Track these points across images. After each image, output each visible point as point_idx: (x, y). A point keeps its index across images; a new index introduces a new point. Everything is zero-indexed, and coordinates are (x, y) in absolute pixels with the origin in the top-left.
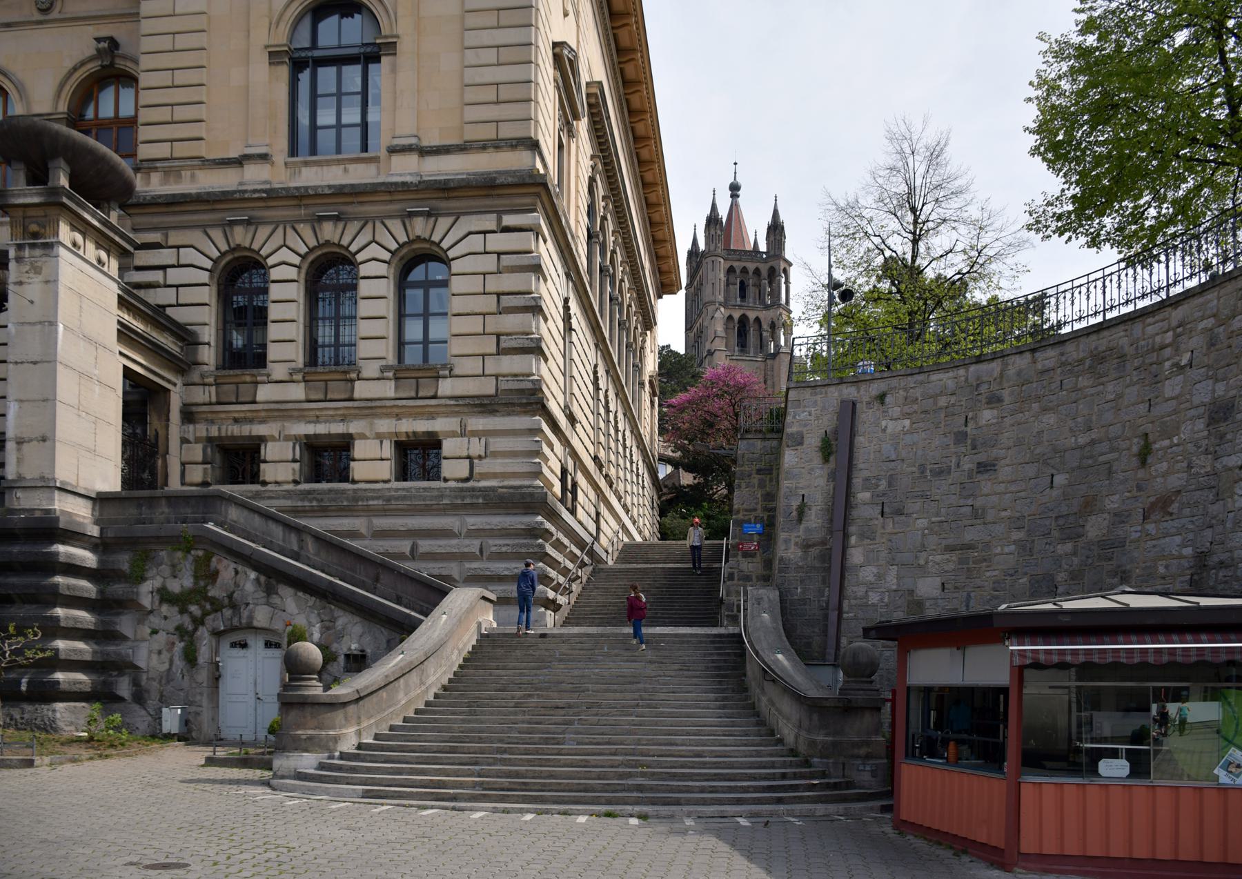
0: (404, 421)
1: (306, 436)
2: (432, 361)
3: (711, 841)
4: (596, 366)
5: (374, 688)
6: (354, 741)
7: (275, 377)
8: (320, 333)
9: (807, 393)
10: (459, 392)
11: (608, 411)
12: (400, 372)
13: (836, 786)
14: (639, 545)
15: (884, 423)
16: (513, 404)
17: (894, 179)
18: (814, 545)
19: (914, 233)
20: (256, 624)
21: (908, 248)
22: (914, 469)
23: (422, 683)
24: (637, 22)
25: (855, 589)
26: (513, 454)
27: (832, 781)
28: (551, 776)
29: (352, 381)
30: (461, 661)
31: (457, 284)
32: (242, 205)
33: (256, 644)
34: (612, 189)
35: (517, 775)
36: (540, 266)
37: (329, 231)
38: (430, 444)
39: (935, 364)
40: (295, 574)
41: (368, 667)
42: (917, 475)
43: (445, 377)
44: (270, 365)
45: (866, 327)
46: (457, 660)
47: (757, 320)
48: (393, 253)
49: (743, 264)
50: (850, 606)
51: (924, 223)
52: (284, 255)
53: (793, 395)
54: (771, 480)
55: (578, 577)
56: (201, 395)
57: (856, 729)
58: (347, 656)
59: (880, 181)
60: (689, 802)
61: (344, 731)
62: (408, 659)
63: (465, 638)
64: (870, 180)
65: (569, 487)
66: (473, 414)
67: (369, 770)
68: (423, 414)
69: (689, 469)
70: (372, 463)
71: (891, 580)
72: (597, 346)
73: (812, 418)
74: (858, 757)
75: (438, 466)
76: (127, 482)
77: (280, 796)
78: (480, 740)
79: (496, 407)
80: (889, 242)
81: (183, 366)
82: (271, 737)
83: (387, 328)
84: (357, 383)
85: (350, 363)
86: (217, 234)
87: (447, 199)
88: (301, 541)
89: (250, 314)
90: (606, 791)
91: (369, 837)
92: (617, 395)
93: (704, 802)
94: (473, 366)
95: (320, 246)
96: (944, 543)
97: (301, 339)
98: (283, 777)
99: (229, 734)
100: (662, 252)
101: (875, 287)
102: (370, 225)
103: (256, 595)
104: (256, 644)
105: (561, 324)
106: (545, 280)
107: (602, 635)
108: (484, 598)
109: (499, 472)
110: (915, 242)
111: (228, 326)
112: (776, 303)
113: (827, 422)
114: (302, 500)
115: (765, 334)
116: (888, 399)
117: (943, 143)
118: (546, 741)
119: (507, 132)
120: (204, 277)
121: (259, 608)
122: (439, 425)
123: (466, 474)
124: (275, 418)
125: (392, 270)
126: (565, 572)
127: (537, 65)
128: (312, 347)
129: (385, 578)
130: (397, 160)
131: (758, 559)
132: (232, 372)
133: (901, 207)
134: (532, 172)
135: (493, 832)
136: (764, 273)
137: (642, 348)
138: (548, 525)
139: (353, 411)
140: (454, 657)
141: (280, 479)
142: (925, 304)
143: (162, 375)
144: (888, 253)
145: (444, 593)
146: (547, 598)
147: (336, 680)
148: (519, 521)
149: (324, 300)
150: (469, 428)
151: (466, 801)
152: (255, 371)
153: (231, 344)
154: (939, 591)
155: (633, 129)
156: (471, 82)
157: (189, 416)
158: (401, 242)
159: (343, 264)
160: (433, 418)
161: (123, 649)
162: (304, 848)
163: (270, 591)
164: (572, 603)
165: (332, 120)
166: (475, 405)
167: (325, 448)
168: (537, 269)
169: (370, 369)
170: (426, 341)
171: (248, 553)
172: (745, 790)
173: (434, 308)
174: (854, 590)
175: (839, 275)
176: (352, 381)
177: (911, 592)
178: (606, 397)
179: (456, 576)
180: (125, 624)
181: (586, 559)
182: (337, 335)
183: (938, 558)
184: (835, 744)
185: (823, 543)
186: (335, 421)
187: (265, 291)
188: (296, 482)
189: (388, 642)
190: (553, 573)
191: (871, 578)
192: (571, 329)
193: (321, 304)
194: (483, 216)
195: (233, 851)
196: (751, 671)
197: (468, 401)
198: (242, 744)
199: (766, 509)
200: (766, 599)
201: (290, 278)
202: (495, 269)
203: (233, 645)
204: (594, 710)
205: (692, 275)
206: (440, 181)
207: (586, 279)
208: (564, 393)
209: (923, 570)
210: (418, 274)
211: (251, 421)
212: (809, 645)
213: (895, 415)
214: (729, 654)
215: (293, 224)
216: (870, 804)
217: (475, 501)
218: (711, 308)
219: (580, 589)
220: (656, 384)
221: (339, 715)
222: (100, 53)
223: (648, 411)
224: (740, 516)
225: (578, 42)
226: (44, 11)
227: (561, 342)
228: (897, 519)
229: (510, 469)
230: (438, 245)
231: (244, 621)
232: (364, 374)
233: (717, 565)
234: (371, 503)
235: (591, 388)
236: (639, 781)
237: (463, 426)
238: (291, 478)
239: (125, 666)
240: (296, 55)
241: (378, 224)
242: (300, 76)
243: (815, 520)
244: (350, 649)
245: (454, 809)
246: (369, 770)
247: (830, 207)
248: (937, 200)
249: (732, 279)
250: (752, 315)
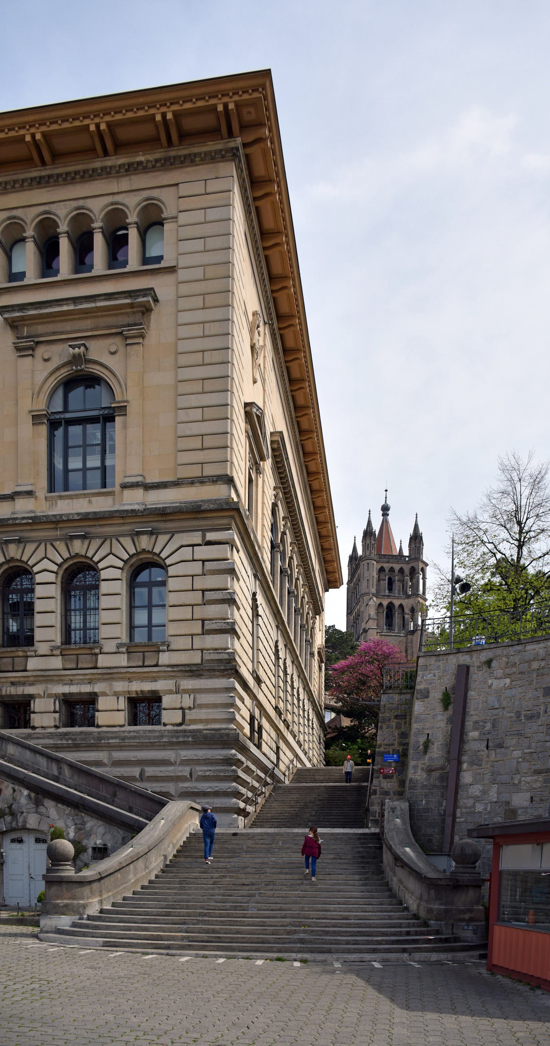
0: (134, 683)
1: (64, 694)
2: (154, 640)
3: (352, 978)
4: (277, 642)
5: (112, 871)
6: (98, 907)
7: (40, 652)
8: (73, 620)
9: (433, 660)
10: (174, 662)
11: (286, 673)
12: (130, 648)
13: (446, 940)
14: (309, 770)
15: (490, 682)
16: (214, 670)
17: (505, 500)
18: (435, 770)
19: (519, 540)
20: (28, 826)
21: (515, 552)
22: (512, 715)
23: (146, 867)
24: (310, 386)
25: (465, 801)
26: (215, 706)
27: (443, 937)
28: (238, 932)
29: (96, 655)
30: (175, 852)
31: (172, 584)
32: (13, 529)
33: (29, 840)
34: (290, 512)
35: (214, 931)
36: (234, 570)
37: (78, 547)
38: (154, 699)
39: (533, 637)
40: (56, 792)
41: (108, 856)
42: (514, 719)
43: (164, 651)
44: (36, 644)
45: (480, 611)
46: (171, 852)
47: (401, 606)
48: (125, 562)
49: (390, 565)
50: (462, 813)
51: (527, 533)
52: (46, 564)
53: (421, 661)
54: (405, 723)
55: (262, 793)
57: (463, 900)
58: (94, 849)
59: (494, 501)
60: (337, 951)
61: (90, 901)
62: (136, 851)
63: (178, 836)
64: (485, 500)
65: (256, 729)
66: (185, 677)
67: (108, 928)
68: (148, 678)
69: (347, 715)
70: (111, 713)
71: (493, 795)
72: (277, 627)
73: (436, 678)
74: (463, 920)
75: (159, 715)
77: (45, 945)
78: (188, 907)
79: (201, 672)
80: (500, 547)
82: (40, 904)
83: (122, 616)
84: (100, 657)
85: (95, 642)
87: (165, 521)
88: (60, 768)
89: (22, 607)
90: (278, 943)
91: (106, 974)
92: (293, 662)
93: (349, 951)
94: (185, 643)
95: (71, 558)
96: (533, 768)
97: (58, 625)
98: (47, 932)
99: (11, 902)
100: (328, 557)
101: (489, 580)
102: (108, 542)
103: (28, 806)
104: (29, 840)
105: (250, 612)
106: (238, 580)
107: (278, 834)
108: (192, 808)
109: (204, 719)
110: (520, 547)
111: (6, 616)
112: (415, 594)
113: (448, 681)
114: (61, 739)
115: (406, 616)
116: (494, 664)
117: (543, 472)
118: (235, 908)
119: (210, 471)
121: (30, 815)
122: (160, 686)
123: (179, 720)
124: (41, 682)
125: (125, 574)
126: (253, 789)
127: (233, 420)
128: (67, 630)
129: (121, 794)
130: (127, 493)
131: (395, 779)
132: (9, 649)
133: (510, 520)
134: (228, 501)
135: (194, 971)
136: (407, 571)
137: (312, 628)
138: (240, 756)
139: (97, 676)
140: (170, 849)
141: (44, 725)
142: (526, 593)
144: (499, 556)
145: (162, 805)
146: (239, 808)
147: (87, 865)
149: (75, 596)
150: (182, 688)
151: (176, 949)
152: (25, 648)
153: (8, 629)
154: (528, 803)
155: (306, 466)
156: (183, 434)
158: (131, 553)
159: (89, 571)
160: (156, 681)
162: (59, 981)
163: (38, 803)
164: (258, 811)
165: (79, 465)
166: (186, 671)
167: (77, 703)
168: (232, 572)
169: (109, 646)
170: (150, 625)
171: (21, 777)
172: (379, 943)
173: (156, 600)
174: (465, 802)
175: (460, 573)
176: (96, 655)
177: (508, 803)
178: (285, 664)
179: (173, 792)
181: (268, 780)
182: (85, 622)
183: (529, 779)
184: (446, 911)
185: (442, 768)
186: (84, 683)
187: (32, 591)
188: (56, 727)
189: (123, 839)
190: (243, 790)
191: (478, 793)
192: (258, 615)
193: (73, 599)
194: (191, 534)
195: (9, 983)
196: (387, 857)
197: (180, 668)
198: (19, 909)
199: (401, 744)
200: (399, 808)
201: (50, 581)
202: (200, 572)
203: (13, 841)
204: (270, 887)
205: (352, 574)
206: (160, 508)
207: (269, 579)
208: (253, 662)
209: (517, 788)
210: (144, 576)
211: (24, 684)
212: (430, 841)
213: (499, 676)
214: (370, 847)
215: (51, 542)
216: (472, 953)
217: (186, 739)
218: (366, 598)
219: (264, 801)
220: (323, 654)
221: (86, 890)
223: (317, 674)
224: (382, 749)
225: (264, 402)
227: (250, 626)
228: (498, 751)
229: (211, 717)
230: (158, 555)
231: (20, 824)
232: (105, 650)
233: (366, 784)
234: (111, 741)
235: (273, 657)
236: (302, 936)
237: (177, 686)
238: (53, 724)
240: (52, 417)
241: (114, 541)
242: (56, 433)
243: (436, 752)
244: (95, 844)
245: (167, 954)
246: (108, 928)
247: (455, 522)
248: (537, 516)
249: (382, 577)
250: (397, 603)
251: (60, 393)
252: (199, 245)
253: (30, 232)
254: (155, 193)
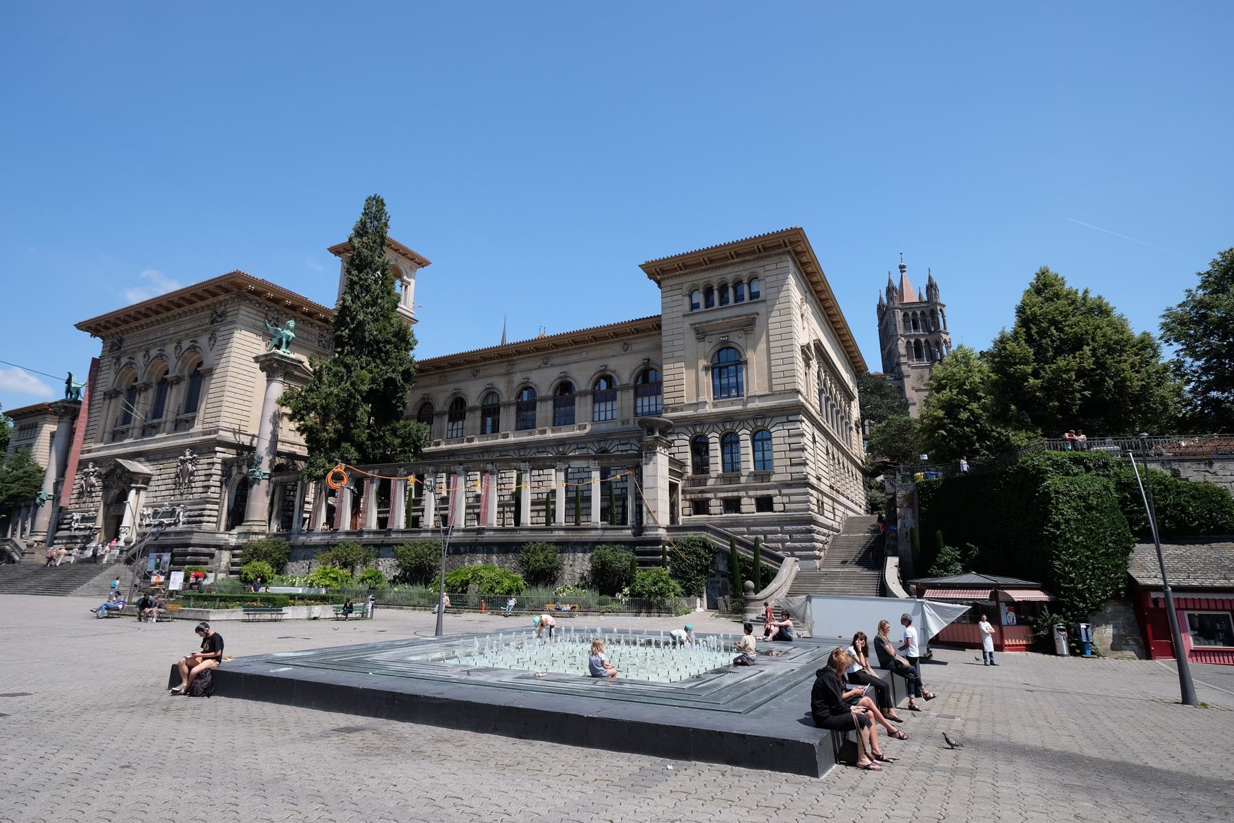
31: (774, 441)
70: (748, 506)
119: (788, 387)
126: (822, 542)
136: (927, 313)
250: (923, 340)
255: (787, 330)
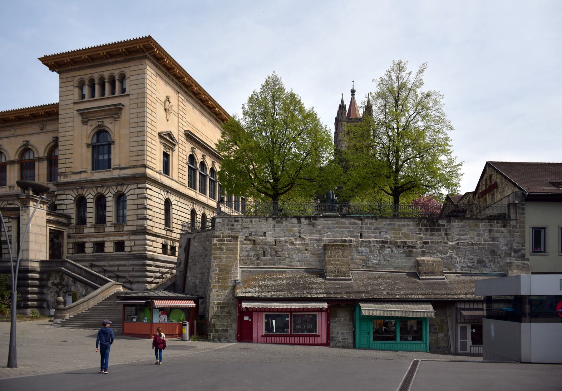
10: (128, 230)
37: (99, 190)
56: (72, 231)
70: (109, 248)
76: (51, 256)
81: (67, 225)
86: (75, 191)
119: (140, 163)
120: (72, 202)
122: (124, 238)
143: (61, 228)
148: (141, 262)
157: (69, 237)
161: (45, 296)
163: (75, 283)
180: (45, 291)
211: (83, 238)
215: (91, 188)
221: (65, 312)
222: (54, 141)
226: (42, 130)
239: (45, 300)
251: (95, 137)
252: (136, 87)
253: (87, 83)
254: (123, 70)
255: (141, 120)
